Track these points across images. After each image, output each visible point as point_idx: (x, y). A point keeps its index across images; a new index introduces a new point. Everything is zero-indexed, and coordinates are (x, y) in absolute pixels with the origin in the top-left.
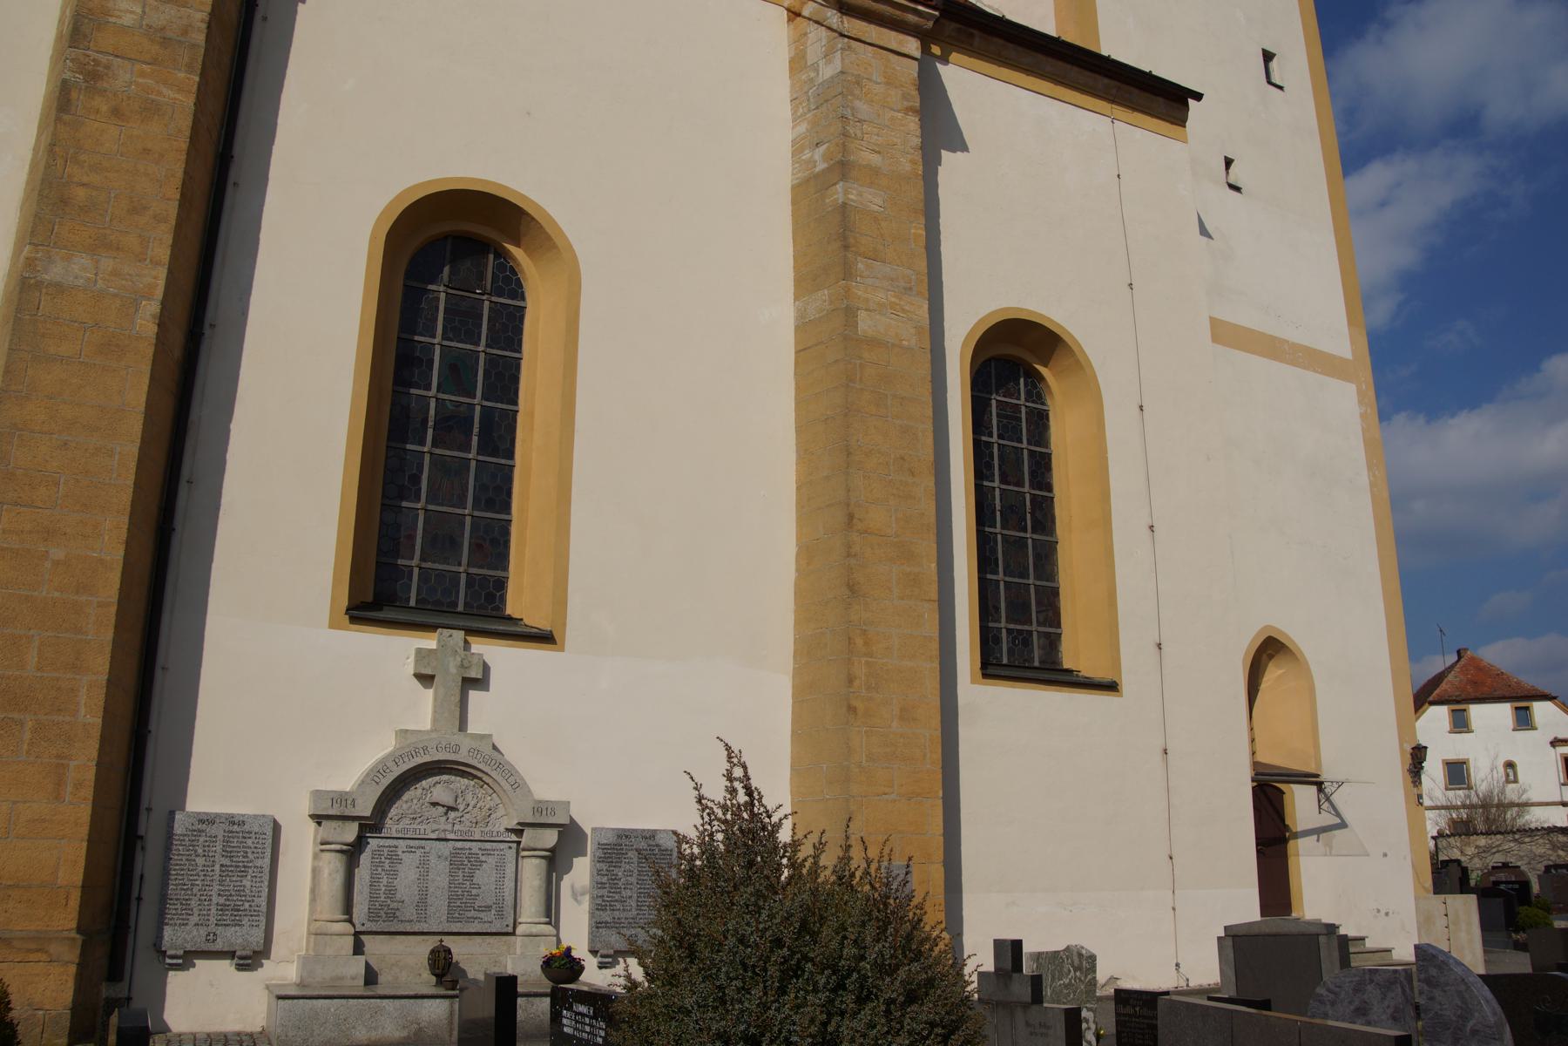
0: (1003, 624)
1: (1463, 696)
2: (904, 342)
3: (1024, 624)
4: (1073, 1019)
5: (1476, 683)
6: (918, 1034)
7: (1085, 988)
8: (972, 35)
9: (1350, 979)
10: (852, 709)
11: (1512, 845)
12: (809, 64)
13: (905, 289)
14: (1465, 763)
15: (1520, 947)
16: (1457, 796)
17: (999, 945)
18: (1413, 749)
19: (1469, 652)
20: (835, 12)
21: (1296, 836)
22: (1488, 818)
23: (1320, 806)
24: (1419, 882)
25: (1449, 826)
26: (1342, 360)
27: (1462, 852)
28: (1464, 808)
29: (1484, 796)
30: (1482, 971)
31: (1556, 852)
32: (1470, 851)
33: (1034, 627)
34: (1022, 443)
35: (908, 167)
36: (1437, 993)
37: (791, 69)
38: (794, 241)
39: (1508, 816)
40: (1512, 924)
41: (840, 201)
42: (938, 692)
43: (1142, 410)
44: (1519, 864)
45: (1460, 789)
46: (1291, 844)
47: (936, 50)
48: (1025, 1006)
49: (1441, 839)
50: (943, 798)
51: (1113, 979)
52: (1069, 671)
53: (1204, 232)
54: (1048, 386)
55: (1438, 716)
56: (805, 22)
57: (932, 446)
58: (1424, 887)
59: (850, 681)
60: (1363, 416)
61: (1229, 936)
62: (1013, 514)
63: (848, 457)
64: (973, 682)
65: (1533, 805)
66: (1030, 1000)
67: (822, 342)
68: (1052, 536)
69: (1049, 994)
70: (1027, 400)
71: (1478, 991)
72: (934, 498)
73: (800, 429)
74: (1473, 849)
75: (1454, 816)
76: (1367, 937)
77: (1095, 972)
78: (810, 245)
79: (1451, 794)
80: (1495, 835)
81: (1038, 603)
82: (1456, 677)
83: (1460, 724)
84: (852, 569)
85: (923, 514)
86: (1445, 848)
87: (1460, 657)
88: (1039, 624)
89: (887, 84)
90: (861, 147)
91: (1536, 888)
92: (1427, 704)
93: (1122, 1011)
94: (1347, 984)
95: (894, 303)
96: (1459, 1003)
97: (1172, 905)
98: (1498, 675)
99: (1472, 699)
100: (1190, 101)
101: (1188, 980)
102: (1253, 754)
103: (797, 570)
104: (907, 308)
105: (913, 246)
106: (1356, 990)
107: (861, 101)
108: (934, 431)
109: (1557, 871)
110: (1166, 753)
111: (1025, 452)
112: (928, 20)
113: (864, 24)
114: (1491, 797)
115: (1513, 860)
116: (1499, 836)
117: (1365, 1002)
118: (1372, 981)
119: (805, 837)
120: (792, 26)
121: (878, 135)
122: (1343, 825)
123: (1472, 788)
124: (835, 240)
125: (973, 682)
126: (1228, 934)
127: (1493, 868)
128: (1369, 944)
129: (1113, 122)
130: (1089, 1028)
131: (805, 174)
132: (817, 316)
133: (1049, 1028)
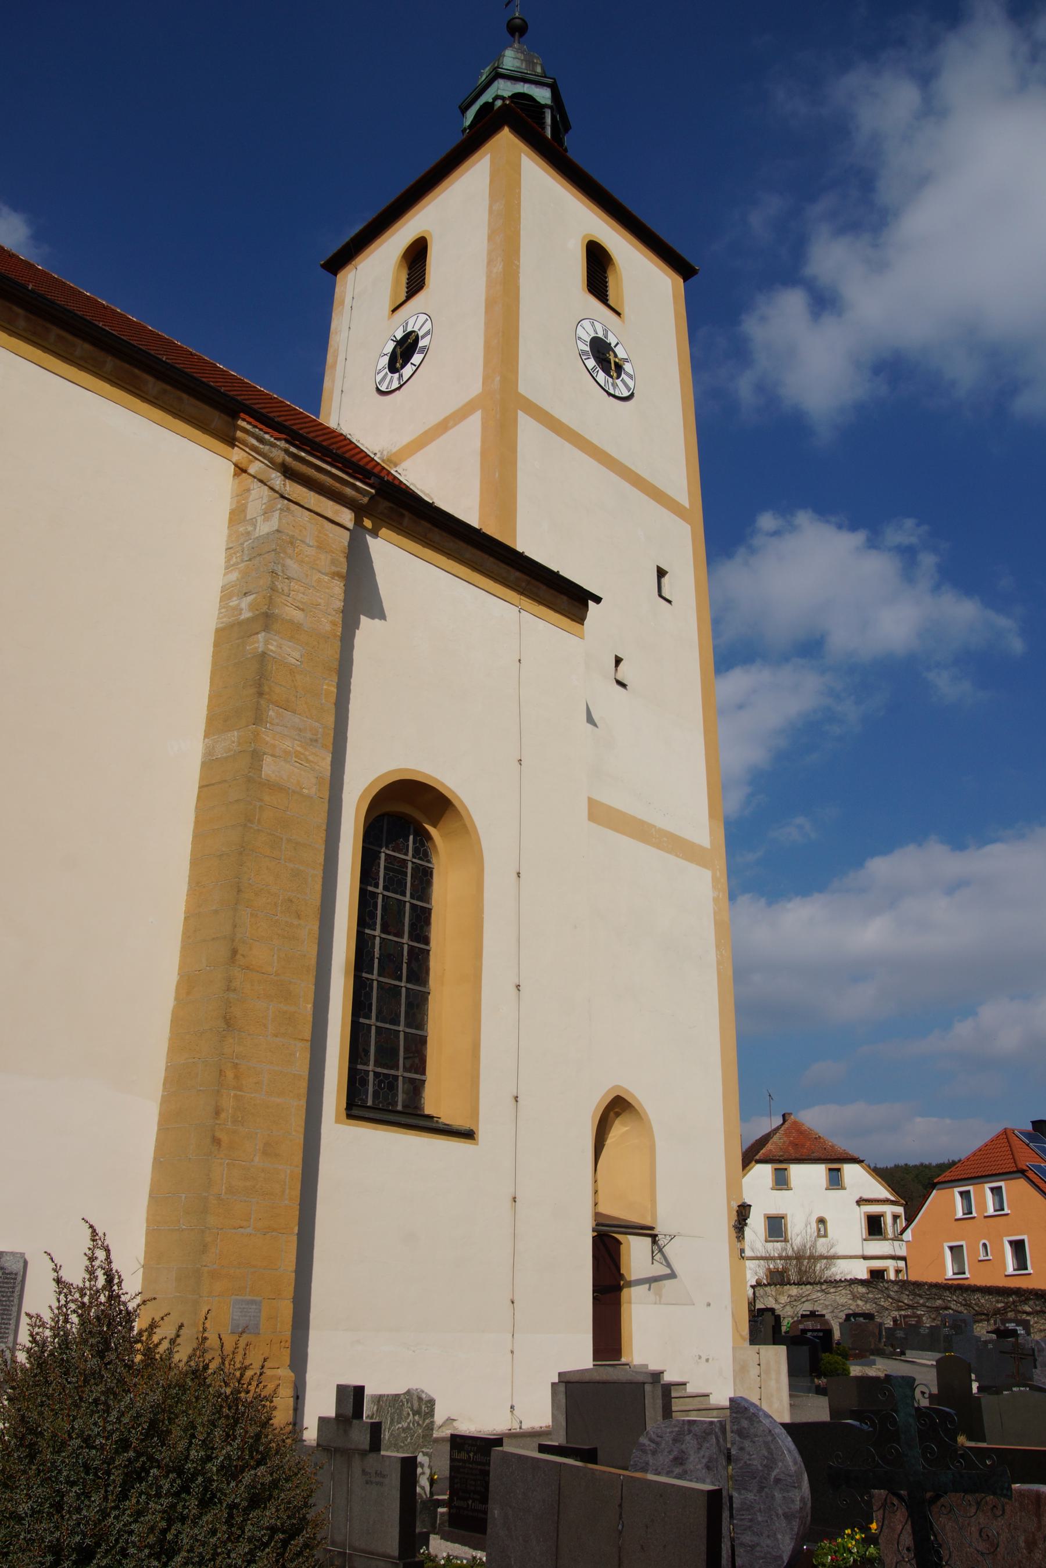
0: (371, 1067)
1: (785, 1157)
2: (304, 790)
3: (391, 1068)
4: (409, 1466)
5: (797, 1145)
6: (258, 1541)
7: (423, 1432)
8: (402, 516)
9: (671, 1430)
10: (216, 1141)
11: (819, 1294)
12: (248, 518)
13: (311, 740)
14: (783, 1218)
15: (820, 1391)
16: (775, 1248)
17: (341, 1390)
18: (739, 1206)
19: (792, 1117)
20: (279, 474)
21: (630, 1284)
22: (800, 1269)
23: (653, 1257)
24: (738, 1331)
25: (767, 1278)
26: (702, 848)
27: (776, 1301)
28: (780, 1260)
29: (798, 1248)
30: (787, 1419)
31: (856, 1302)
32: (784, 1299)
33: (400, 1072)
34: (405, 896)
35: (328, 627)
36: (747, 1444)
37: (231, 520)
38: (211, 678)
39: (818, 1268)
40: (816, 1369)
41: (260, 650)
42: (302, 1130)
43: (519, 877)
44: (824, 1312)
45: (778, 1242)
46: (625, 1292)
47: (368, 523)
48: (363, 1454)
49: (759, 1288)
50: (298, 1234)
51: (450, 1420)
52: (430, 1117)
53: (590, 720)
54: (435, 846)
55: (763, 1172)
56: (251, 479)
57: (320, 892)
58: (741, 1335)
59: (217, 1113)
60: (716, 900)
61: (562, 1382)
62: (390, 962)
63: (238, 894)
64: (338, 1121)
65: (839, 1258)
66: (367, 1448)
67: (225, 781)
68: (425, 987)
69: (387, 1438)
70: (414, 857)
71: (782, 1442)
72: (317, 941)
73: (196, 861)
74: (786, 1298)
75: (771, 1266)
76: (688, 1382)
77: (432, 1416)
78: (226, 687)
79: (770, 1245)
80: (806, 1285)
81: (406, 1050)
82: (780, 1139)
83: (781, 1182)
84: (230, 1003)
85: (305, 956)
86: (762, 1297)
87: (784, 1121)
88: (405, 1070)
89: (318, 547)
90: (285, 602)
91: (837, 1334)
92: (753, 1163)
93: (456, 1456)
94: (668, 1435)
95: (299, 752)
96: (766, 1454)
97: (510, 1348)
98: (816, 1138)
99: (793, 1160)
100: (590, 603)
101: (521, 1422)
102: (595, 1205)
103: (176, 999)
104: (311, 758)
105: (324, 701)
106: (675, 1440)
107: (292, 559)
108: (323, 878)
109: (855, 1320)
110: (515, 1201)
111: (408, 905)
112: (364, 496)
113: (304, 490)
114: (804, 1250)
115: (820, 1309)
116: (808, 1287)
117: (683, 1452)
118: (690, 1432)
119: (162, 1319)
120: (237, 481)
121: (304, 594)
122: (672, 1275)
123: (788, 1242)
124: (251, 686)
125: (338, 1121)
126: (562, 1380)
127: (803, 1316)
128: (690, 1389)
129: (519, 611)
130: (423, 1473)
131: (230, 620)
132: (225, 755)
133: (384, 1476)
